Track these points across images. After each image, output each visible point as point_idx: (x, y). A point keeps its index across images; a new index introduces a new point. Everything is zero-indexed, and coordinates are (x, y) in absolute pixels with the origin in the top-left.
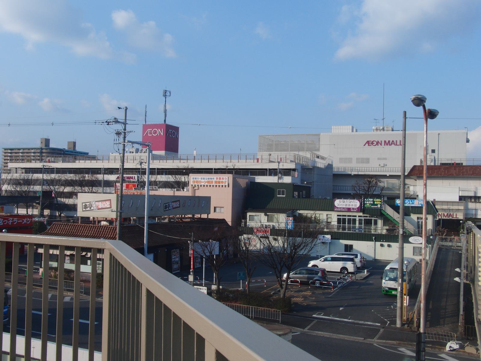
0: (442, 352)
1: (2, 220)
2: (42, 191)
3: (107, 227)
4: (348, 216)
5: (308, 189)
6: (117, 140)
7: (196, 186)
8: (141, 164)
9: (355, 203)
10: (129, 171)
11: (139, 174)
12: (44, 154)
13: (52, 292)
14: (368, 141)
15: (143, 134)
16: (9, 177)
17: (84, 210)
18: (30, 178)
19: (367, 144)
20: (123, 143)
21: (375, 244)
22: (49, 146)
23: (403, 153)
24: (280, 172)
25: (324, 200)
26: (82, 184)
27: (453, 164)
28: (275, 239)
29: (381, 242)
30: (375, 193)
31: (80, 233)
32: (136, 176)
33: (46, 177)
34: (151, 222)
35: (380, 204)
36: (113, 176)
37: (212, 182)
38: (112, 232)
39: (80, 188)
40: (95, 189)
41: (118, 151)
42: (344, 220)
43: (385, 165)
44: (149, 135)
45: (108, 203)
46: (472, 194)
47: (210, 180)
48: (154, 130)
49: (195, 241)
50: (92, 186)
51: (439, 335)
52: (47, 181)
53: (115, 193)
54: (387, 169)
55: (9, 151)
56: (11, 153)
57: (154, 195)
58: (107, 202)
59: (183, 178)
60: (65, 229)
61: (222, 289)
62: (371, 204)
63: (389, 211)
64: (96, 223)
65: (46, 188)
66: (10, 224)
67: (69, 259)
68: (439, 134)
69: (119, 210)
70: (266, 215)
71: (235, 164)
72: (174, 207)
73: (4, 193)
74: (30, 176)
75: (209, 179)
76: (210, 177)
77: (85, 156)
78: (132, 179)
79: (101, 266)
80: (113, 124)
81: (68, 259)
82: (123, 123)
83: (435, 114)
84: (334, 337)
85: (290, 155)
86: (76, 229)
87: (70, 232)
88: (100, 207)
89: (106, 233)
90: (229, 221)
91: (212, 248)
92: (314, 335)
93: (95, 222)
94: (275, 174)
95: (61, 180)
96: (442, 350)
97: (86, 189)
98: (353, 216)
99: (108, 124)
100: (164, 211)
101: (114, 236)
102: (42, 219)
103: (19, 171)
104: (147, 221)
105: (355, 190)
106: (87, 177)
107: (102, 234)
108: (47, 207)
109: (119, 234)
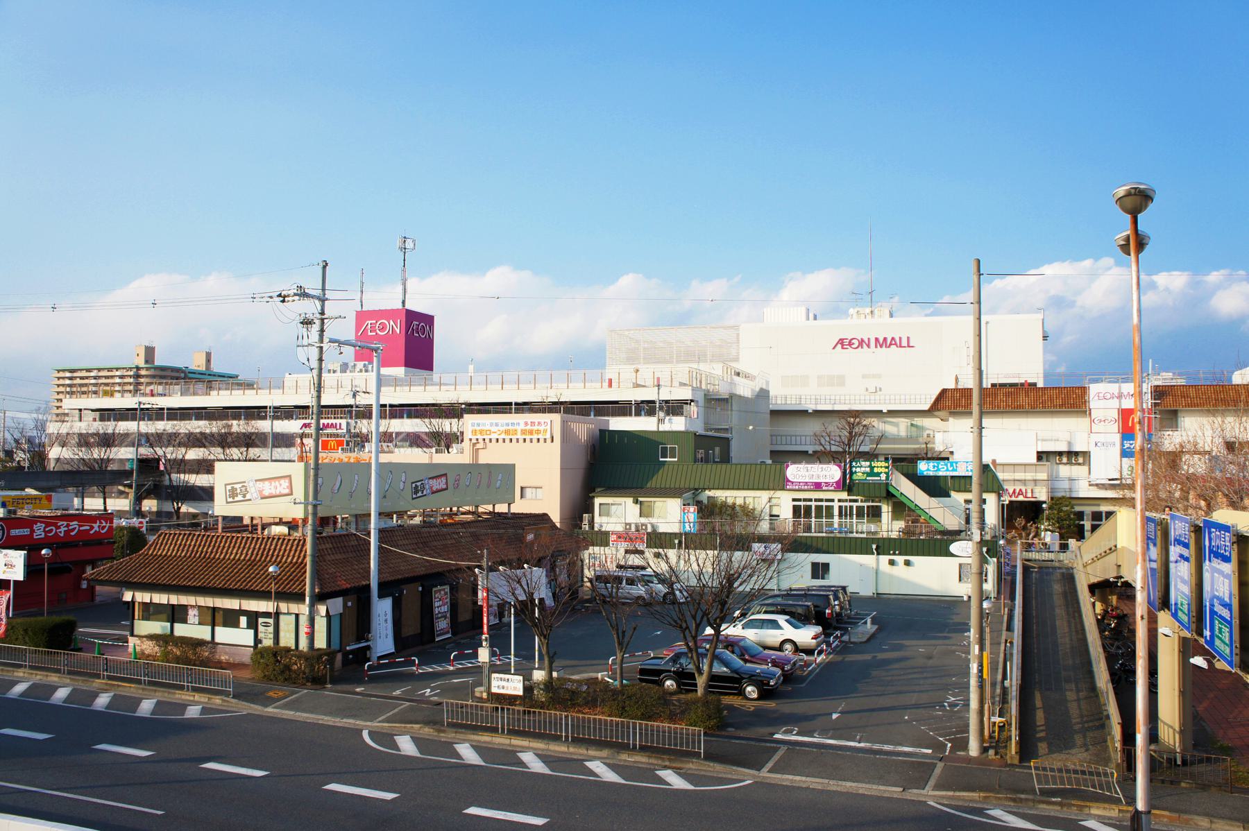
0: (1087, 814)
1: (44, 525)
2: (138, 459)
3: (284, 539)
4: (816, 500)
5: (725, 443)
6: (305, 337)
7: (481, 441)
8: (354, 396)
9: (830, 473)
11: (351, 418)
12: (142, 380)
13: (157, 694)
14: (840, 339)
15: (357, 332)
16: (64, 429)
18: (110, 431)
19: (839, 346)
20: (318, 345)
21: (878, 560)
22: (153, 362)
23: (977, 354)
24: (661, 408)
25: (758, 467)
26: (224, 441)
27: (1022, 384)
28: (657, 555)
29: (890, 554)
30: (863, 449)
31: (222, 553)
32: (344, 422)
33: (145, 427)
34: (383, 525)
36: (292, 422)
37: (515, 432)
38: (296, 551)
39: (219, 450)
40: (254, 452)
41: (306, 363)
42: (808, 509)
43: (878, 389)
44: (370, 334)
45: (285, 483)
46: (1064, 448)
47: (510, 427)
49: (492, 569)
50: (248, 446)
51: (1068, 771)
52: (147, 436)
53: (301, 459)
54: (882, 397)
55: (68, 375)
56: (71, 378)
57: (390, 464)
58: (282, 481)
59: (447, 425)
60: (185, 545)
61: (558, 679)
62: (867, 473)
63: (906, 488)
64: (257, 530)
65: (145, 451)
66: (62, 535)
67: (197, 614)
69: (311, 499)
70: (636, 502)
71: (561, 391)
72: (434, 489)
73: (51, 466)
74: (110, 427)
76: (510, 422)
77: (230, 381)
79: (271, 629)
80: (294, 301)
82: (319, 298)
83: (1144, 241)
84: (834, 788)
85: (682, 371)
86: (212, 544)
87: (197, 552)
88: (266, 493)
89: (281, 553)
90: (556, 518)
91: (534, 584)
92: (787, 786)
93: (254, 527)
94: (651, 412)
95: (179, 434)
96: (1086, 811)
97: (235, 452)
98: (827, 500)
99: (283, 301)
100: (413, 499)
101: (300, 560)
102: (135, 522)
103: (89, 416)
104: (375, 524)
105: (821, 444)
106: (237, 426)
107: (273, 556)
108: (149, 494)
109: (313, 556)
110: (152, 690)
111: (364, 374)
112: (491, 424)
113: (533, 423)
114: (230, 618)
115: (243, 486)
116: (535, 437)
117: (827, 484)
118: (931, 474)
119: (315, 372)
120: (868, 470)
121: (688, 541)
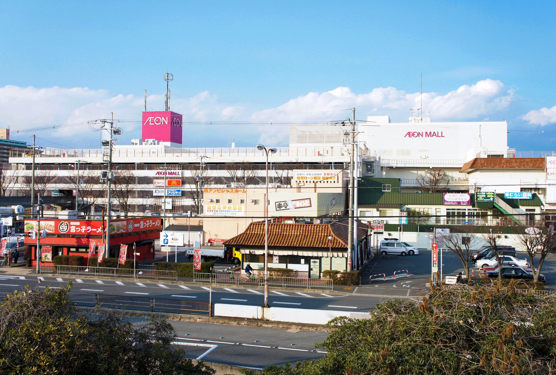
4: (457, 209)
7: (302, 182)
10: (173, 166)
17: (277, 209)
19: (408, 136)
29: (498, 233)
32: (180, 171)
35: (492, 197)
43: (427, 157)
44: (151, 124)
47: (317, 176)
48: (157, 118)
58: (306, 201)
68: (480, 126)
70: (378, 210)
75: (315, 174)
78: (176, 174)
81: (277, 259)
99: (344, 125)
110: (291, 289)
111: (153, 145)
112: (307, 174)
113: (328, 174)
114: (296, 260)
115: (285, 203)
116: (329, 180)
117: (463, 202)
118: (510, 198)
119: (351, 155)
120: (485, 196)
121: (407, 228)
